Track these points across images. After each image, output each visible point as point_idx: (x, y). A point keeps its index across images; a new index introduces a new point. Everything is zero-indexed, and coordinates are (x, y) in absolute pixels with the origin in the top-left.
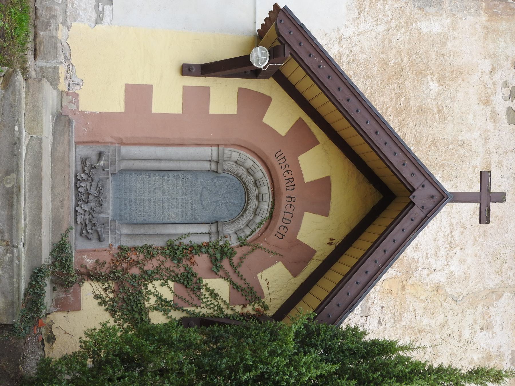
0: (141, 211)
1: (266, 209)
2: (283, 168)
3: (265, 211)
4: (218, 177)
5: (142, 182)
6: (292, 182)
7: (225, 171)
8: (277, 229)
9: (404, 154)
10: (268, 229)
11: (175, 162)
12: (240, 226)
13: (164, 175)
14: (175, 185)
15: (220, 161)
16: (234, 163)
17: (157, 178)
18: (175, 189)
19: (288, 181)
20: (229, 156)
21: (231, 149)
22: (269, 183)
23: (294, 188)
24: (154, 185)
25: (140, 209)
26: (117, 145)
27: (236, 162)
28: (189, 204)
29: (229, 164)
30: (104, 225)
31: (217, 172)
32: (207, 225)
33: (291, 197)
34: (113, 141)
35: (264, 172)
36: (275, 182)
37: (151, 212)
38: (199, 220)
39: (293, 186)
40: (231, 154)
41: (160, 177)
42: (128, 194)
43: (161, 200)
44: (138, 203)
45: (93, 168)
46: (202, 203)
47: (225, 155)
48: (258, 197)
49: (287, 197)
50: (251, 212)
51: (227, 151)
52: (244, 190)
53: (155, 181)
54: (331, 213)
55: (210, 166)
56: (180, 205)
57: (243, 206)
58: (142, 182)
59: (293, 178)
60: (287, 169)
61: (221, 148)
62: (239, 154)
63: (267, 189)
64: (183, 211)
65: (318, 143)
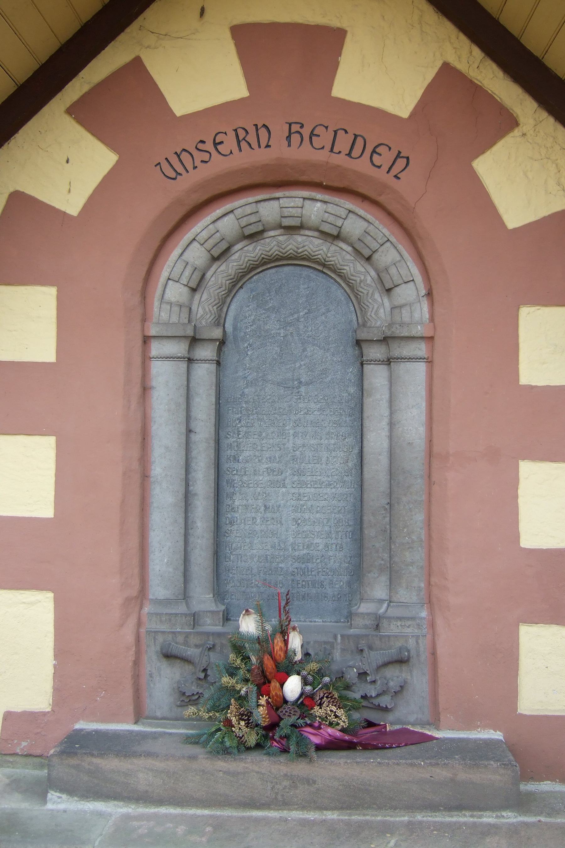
0: (326, 546)
1: (325, 206)
2: (206, 157)
3: (329, 210)
4: (235, 337)
5: (248, 540)
6: (247, 132)
7: (219, 321)
8: (381, 175)
9: (359, 459)
10: (381, 199)
11: (194, 453)
12: (369, 278)
13: (231, 483)
14: (257, 453)
15: (190, 332)
16: (197, 296)
17: (237, 503)
18: (267, 454)
19: (244, 144)
20: (176, 309)
21: (156, 303)
22: (251, 199)
23: (264, 126)
24: (257, 511)
25: (321, 547)
26: (146, 610)
27: (194, 290)
28: (310, 418)
29: (200, 309)
30: (362, 650)
31: (222, 342)
32: (367, 368)
33: (290, 133)
34: (132, 622)
35: (219, 212)
36: (247, 181)
37: (329, 520)
38: (352, 390)
39: (257, 130)
40: (171, 304)
41: (233, 493)
42: (280, 578)
43: (296, 491)
44: (305, 552)
45: (206, 676)
46: (307, 384)
47: (174, 319)
48: (290, 229)
49: (289, 145)
50: (333, 248)
51: (163, 314)
52: (273, 271)
53: (246, 507)
54: (335, 23)
55: (205, 361)
56: (312, 442)
57: (316, 273)
58: (248, 540)
59: (236, 130)
60: (209, 146)
61: (153, 331)
62: (170, 282)
63: (266, 203)
64: (328, 433)
65: (137, 63)
